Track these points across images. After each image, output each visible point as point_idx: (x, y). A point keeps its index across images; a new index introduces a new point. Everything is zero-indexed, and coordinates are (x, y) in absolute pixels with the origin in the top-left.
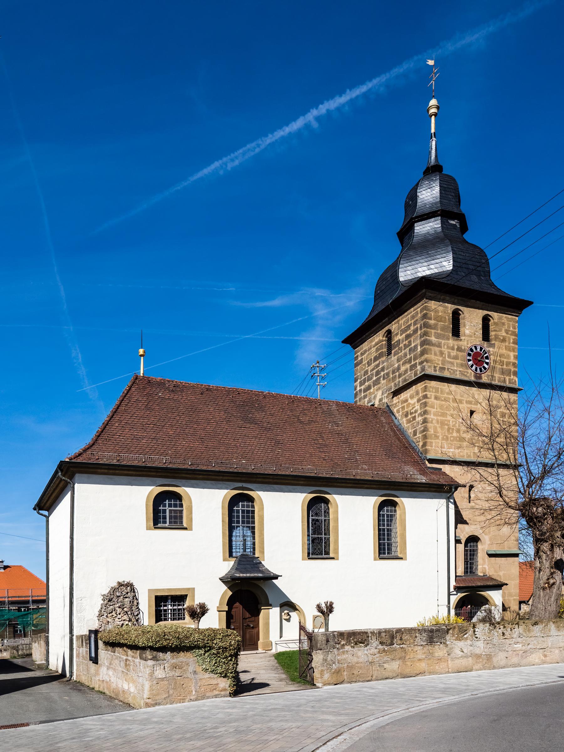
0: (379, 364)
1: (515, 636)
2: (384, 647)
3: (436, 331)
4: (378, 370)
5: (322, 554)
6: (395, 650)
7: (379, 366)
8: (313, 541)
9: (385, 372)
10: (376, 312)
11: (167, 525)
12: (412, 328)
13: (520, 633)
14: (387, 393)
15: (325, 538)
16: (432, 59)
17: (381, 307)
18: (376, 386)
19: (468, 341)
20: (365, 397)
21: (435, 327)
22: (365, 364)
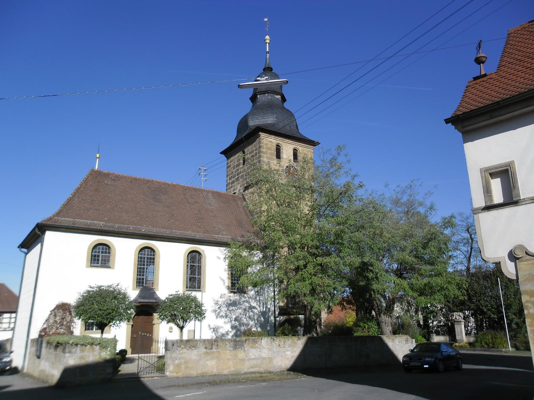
0: (239, 169)
1: (286, 346)
2: (207, 350)
3: (267, 155)
4: (238, 172)
5: (196, 288)
6: (213, 352)
7: (239, 170)
8: (190, 280)
9: (242, 174)
10: (237, 140)
11: (99, 265)
12: (254, 152)
14: (243, 186)
15: (198, 277)
17: (240, 138)
18: (237, 182)
19: (285, 162)
20: (232, 187)
21: (266, 153)
22: (232, 168)
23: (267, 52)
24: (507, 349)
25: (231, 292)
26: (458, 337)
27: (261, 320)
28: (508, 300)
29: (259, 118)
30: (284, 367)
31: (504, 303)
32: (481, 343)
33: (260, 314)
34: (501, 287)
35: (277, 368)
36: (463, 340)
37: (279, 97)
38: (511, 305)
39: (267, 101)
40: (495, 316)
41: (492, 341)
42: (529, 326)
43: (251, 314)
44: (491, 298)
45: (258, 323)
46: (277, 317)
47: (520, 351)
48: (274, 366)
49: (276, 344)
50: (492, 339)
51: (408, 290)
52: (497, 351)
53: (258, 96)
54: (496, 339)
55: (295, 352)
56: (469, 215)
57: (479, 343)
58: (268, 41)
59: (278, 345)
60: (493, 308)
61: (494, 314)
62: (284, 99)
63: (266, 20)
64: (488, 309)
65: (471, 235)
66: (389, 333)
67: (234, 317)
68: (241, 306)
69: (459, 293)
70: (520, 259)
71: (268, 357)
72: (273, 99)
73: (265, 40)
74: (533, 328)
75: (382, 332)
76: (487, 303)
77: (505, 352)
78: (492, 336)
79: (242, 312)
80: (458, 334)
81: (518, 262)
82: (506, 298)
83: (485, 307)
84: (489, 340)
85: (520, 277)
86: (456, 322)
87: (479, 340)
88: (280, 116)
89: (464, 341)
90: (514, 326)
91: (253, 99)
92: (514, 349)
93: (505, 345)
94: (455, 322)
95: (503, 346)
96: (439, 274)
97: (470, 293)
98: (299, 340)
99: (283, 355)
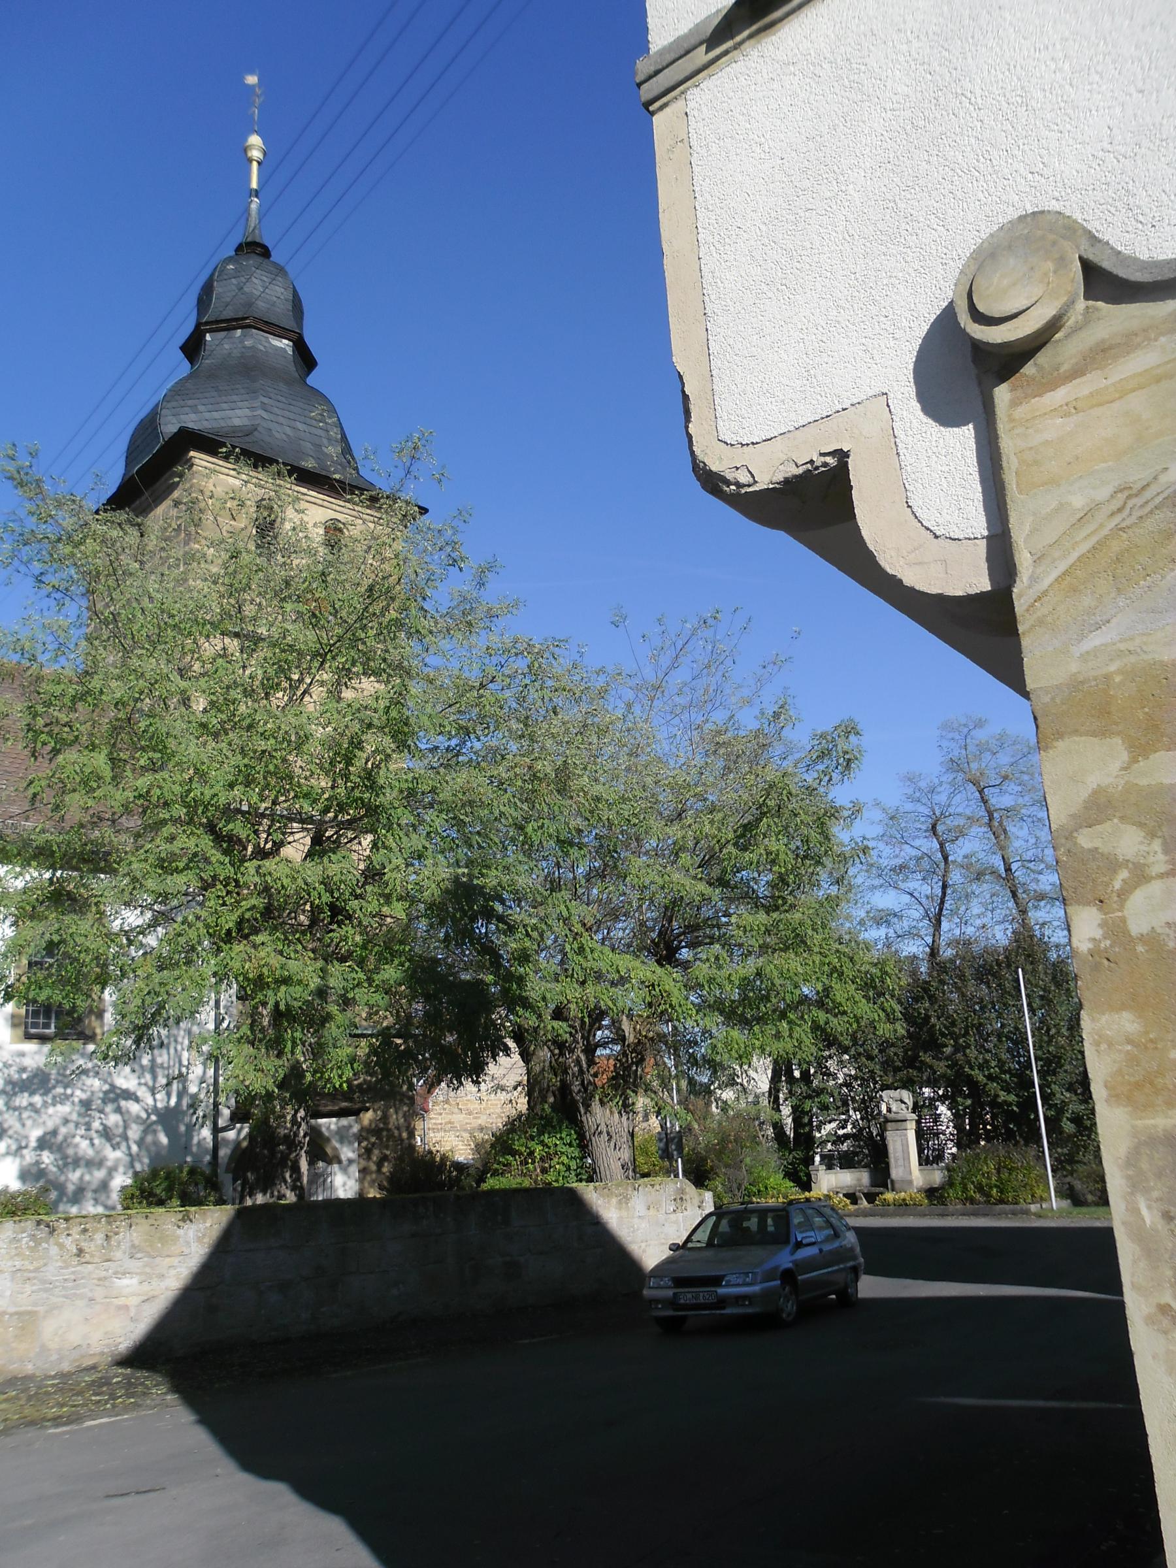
1: (118, 1254)
13: (133, 1246)
16: (252, 72)
23: (253, 193)
24: (1044, 1206)
25: (28, 1037)
26: (896, 1173)
27: (156, 1143)
28: (1049, 1042)
29: (201, 408)
30: (98, 1350)
31: (1039, 1053)
32: (965, 1189)
33: (154, 1118)
34: (1029, 1005)
35: (61, 1360)
36: (910, 1182)
37: (285, 344)
38: (1060, 1058)
39: (239, 355)
40: (1012, 1098)
41: (1000, 1179)
42: (1115, 1097)
43: (113, 1119)
44: (1000, 1041)
45: (144, 1153)
46: (225, 1129)
47: (1084, 1210)
48: (44, 1349)
49: (61, 1246)
50: (999, 1172)
51: (680, 1006)
52: (1014, 1213)
53: (208, 337)
54: (1010, 1174)
55: (162, 1276)
56: (936, 781)
57: (959, 1188)
58: (256, 154)
59: (75, 1251)
60: (1005, 1072)
61: (1008, 1090)
62: (305, 359)
63: (252, 80)
64: (990, 1075)
65: (942, 845)
66: (618, 1172)
67: (35, 1134)
68: (69, 1091)
69: (875, 1014)
70: (1029, 369)
71: (12, 1310)
72: (262, 348)
73: (245, 150)
74: (1162, 1121)
75: (595, 1172)
76: (988, 1056)
77: (1039, 1216)
78: (1000, 1164)
79: (74, 1117)
80: (896, 1160)
81: (1014, 403)
82: (1046, 1038)
83: (981, 1067)
84: (989, 1178)
85: (1024, 559)
86: (892, 1121)
87: (959, 1179)
88: (278, 404)
89: (915, 1183)
90: (1068, 1127)
91: (192, 348)
92: (1066, 1203)
93: (1039, 1192)
94: (887, 1121)
95: (1033, 1196)
96: (797, 942)
97: (934, 1026)
98: (188, 1225)
99: (99, 1293)
